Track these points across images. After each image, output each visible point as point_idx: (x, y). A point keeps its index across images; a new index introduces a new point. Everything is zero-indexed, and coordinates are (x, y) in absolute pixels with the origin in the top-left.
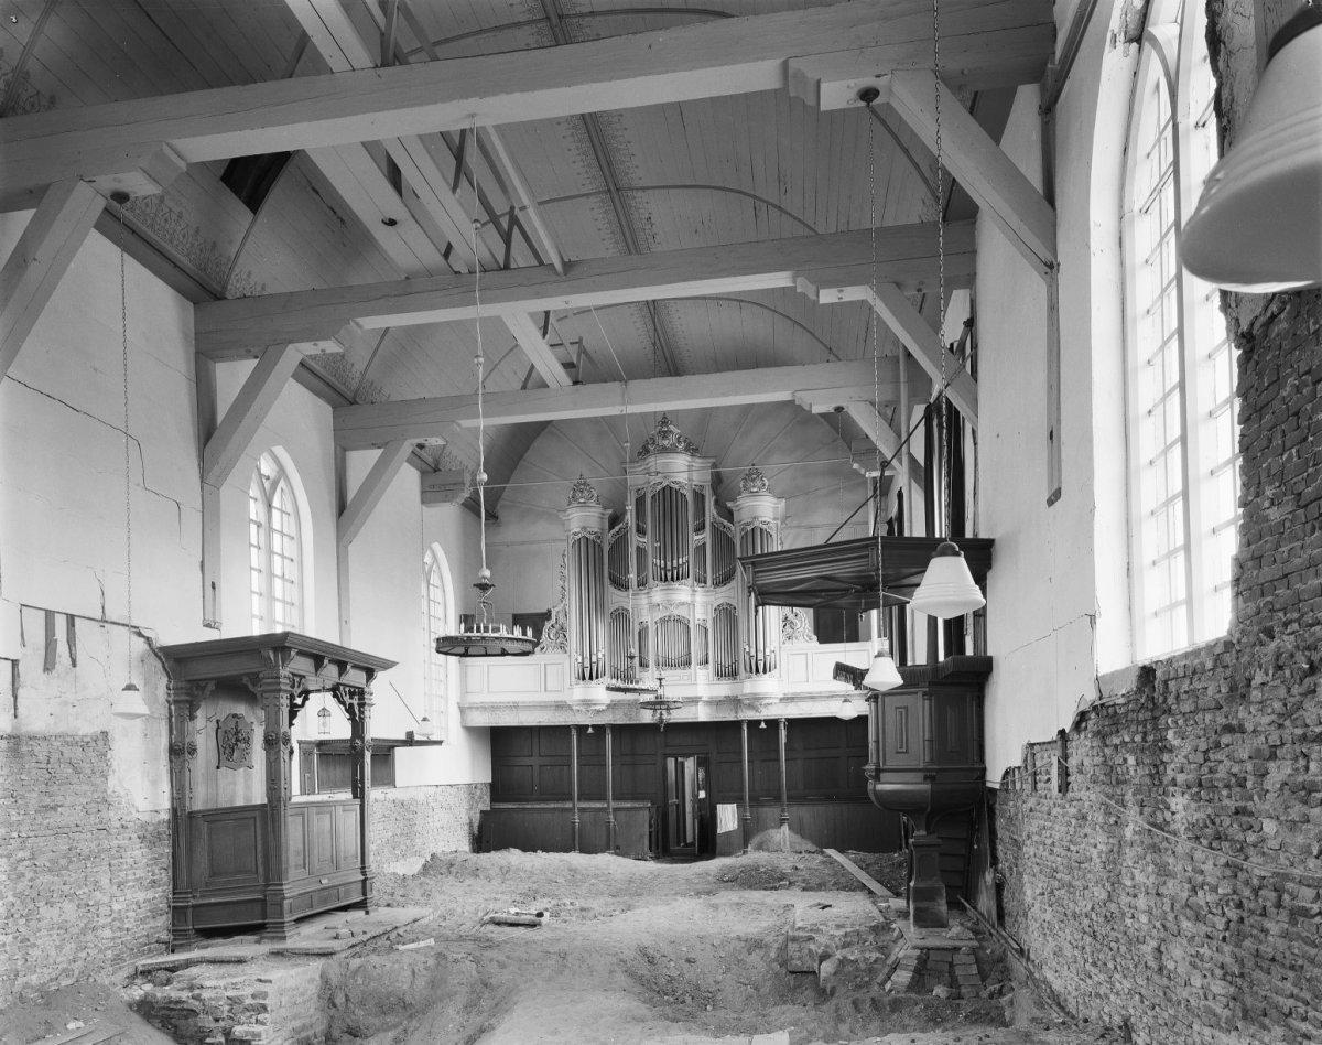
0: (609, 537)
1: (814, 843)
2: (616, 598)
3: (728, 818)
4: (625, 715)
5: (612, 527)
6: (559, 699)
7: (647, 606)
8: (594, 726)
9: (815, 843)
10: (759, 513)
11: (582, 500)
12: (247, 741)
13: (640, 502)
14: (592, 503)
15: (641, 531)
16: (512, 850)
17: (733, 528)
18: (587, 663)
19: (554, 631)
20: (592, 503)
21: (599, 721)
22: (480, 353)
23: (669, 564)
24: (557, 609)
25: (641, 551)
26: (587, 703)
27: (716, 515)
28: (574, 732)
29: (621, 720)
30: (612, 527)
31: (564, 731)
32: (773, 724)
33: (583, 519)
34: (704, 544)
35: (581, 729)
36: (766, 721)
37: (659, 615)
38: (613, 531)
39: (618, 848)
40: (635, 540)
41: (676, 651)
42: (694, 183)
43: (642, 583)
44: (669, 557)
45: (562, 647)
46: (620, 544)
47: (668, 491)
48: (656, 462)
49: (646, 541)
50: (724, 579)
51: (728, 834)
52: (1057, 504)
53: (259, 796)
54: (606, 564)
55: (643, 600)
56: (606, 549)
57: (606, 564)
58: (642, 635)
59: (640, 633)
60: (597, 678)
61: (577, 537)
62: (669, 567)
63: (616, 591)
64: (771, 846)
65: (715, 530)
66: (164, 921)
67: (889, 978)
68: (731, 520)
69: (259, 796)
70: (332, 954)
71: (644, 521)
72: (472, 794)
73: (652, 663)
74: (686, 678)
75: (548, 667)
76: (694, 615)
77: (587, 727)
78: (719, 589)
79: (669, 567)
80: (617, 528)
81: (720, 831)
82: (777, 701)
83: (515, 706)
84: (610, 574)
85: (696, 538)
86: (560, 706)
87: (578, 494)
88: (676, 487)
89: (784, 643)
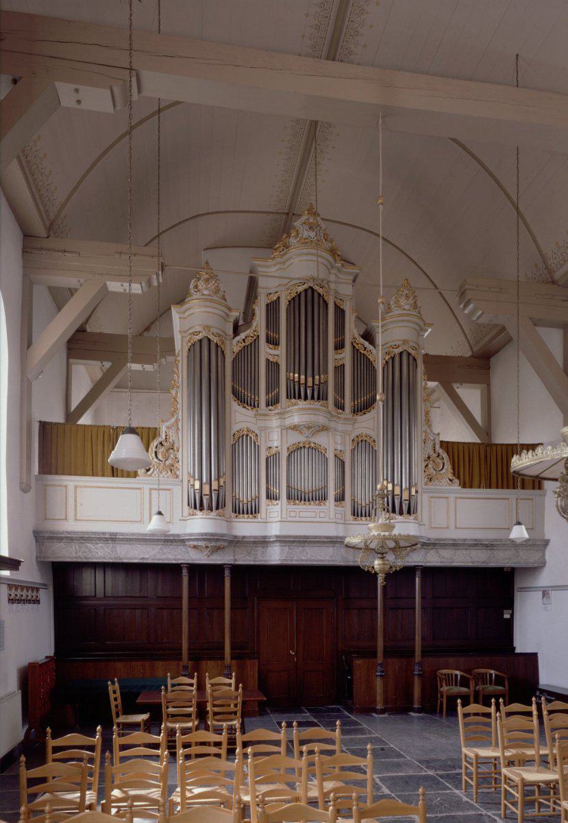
12: (232, 726)
13: (272, 308)
15: (273, 341)
17: (374, 351)
18: (206, 490)
19: (161, 450)
27: (357, 335)
34: (343, 366)
38: (237, 338)
40: (266, 352)
43: (273, 402)
45: (172, 468)
55: (275, 422)
59: (267, 459)
62: (310, 383)
67: (169, 747)
70: (207, 249)
72: (470, 739)
74: (322, 515)
79: (310, 383)
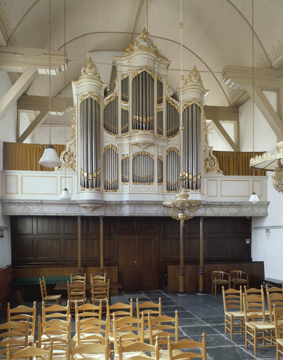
13: (125, 82)
15: (125, 100)
16: (256, 257)
17: (178, 104)
19: (67, 156)
23: (144, 119)
28: (79, 220)
31: (73, 219)
38: (106, 98)
40: (121, 105)
43: (125, 131)
45: (72, 166)
52: (265, 151)
53: (173, 351)
54: (99, 119)
55: (126, 141)
56: (102, 109)
59: (122, 161)
60: (96, 187)
61: (85, 98)
62: (144, 121)
66: (253, 225)
69: (173, 351)
71: (127, 94)
74: (151, 190)
79: (144, 121)
83: (41, 203)
84: (104, 123)
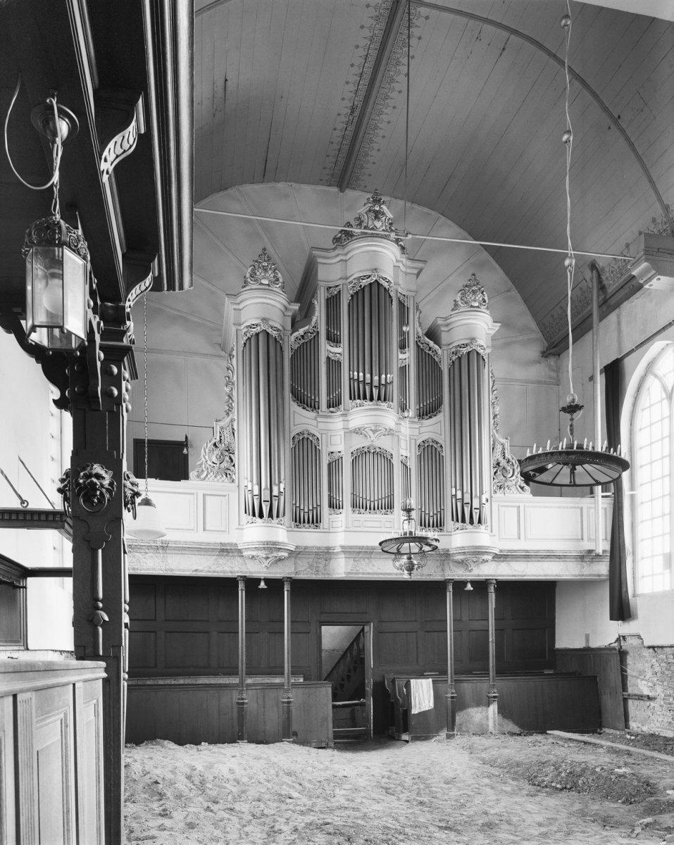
0: (291, 341)
1: (517, 723)
2: (300, 419)
3: (422, 695)
4: (311, 566)
5: (295, 325)
6: (226, 541)
7: (342, 433)
8: (267, 581)
9: (521, 725)
10: (476, 335)
11: (266, 282)
13: (333, 303)
14: (276, 288)
17: (440, 352)
18: (265, 496)
20: (276, 288)
21: (278, 572)
22: (569, 126)
23: (376, 378)
24: (221, 424)
25: (334, 365)
26: (271, 547)
28: (241, 586)
29: (305, 572)
30: (295, 325)
32: (481, 586)
33: (260, 307)
35: (252, 583)
36: (473, 583)
37: (359, 443)
38: (296, 334)
39: (295, 734)
41: (374, 492)
42: (598, 92)
43: (334, 403)
44: (375, 370)
46: (306, 352)
47: (375, 288)
48: (359, 249)
49: (340, 351)
50: (428, 411)
51: (423, 714)
56: (287, 355)
57: (288, 374)
58: (334, 466)
59: (329, 465)
62: (376, 383)
63: (300, 410)
64: (473, 728)
65: (420, 351)
68: (437, 341)
73: (347, 499)
75: (207, 498)
76: (347, 519)
77: (258, 581)
78: (427, 422)
80: (301, 331)
81: (415, 711)
82: (490, 557)
85: (401, 356)
86: (226, 551)
87: (259, 273)
88: (386, 284)
89: (495, 492)
